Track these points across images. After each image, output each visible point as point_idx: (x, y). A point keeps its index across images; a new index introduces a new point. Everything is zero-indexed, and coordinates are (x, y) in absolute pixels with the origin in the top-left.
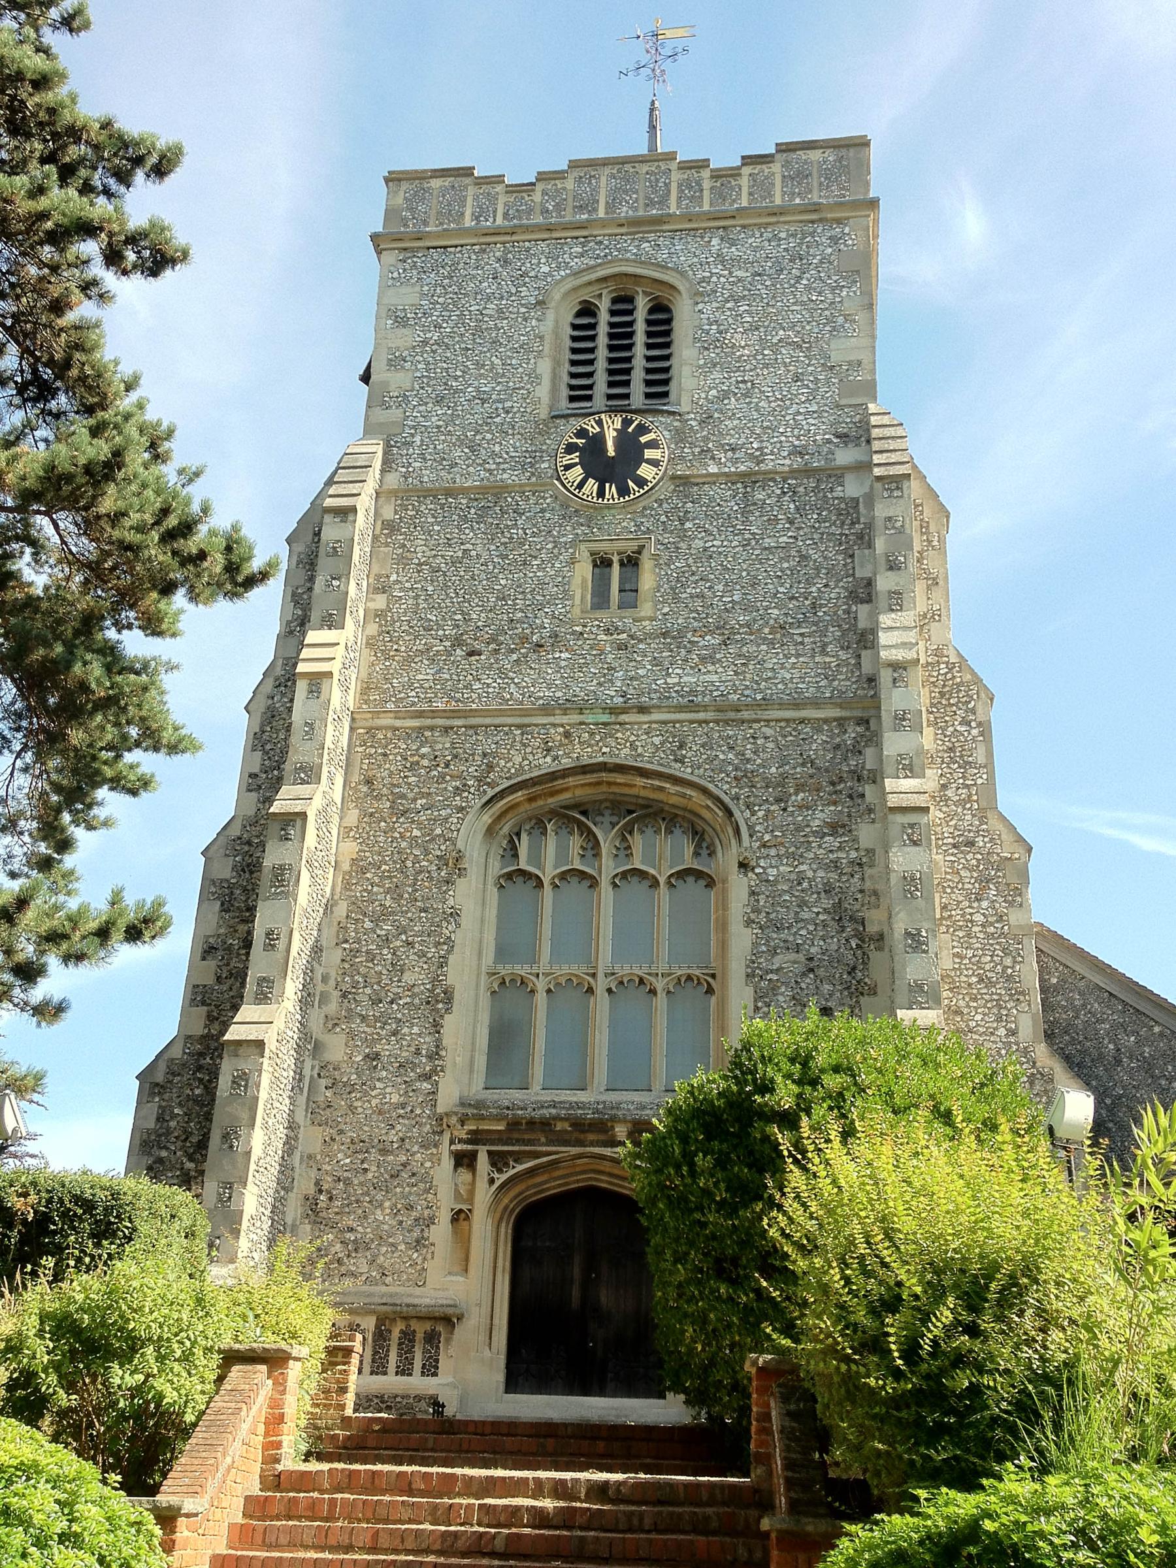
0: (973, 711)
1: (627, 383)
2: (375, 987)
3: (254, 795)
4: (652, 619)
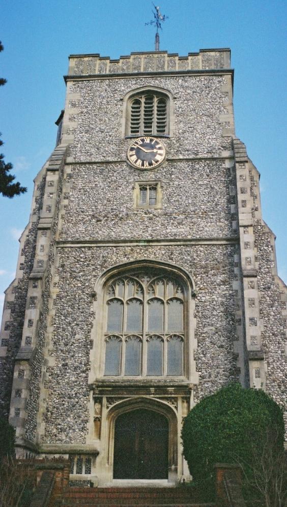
0: (269, 242)
1: (151, 127)
2: (66, 340)
3: (22, 271)
4: (161, 209)
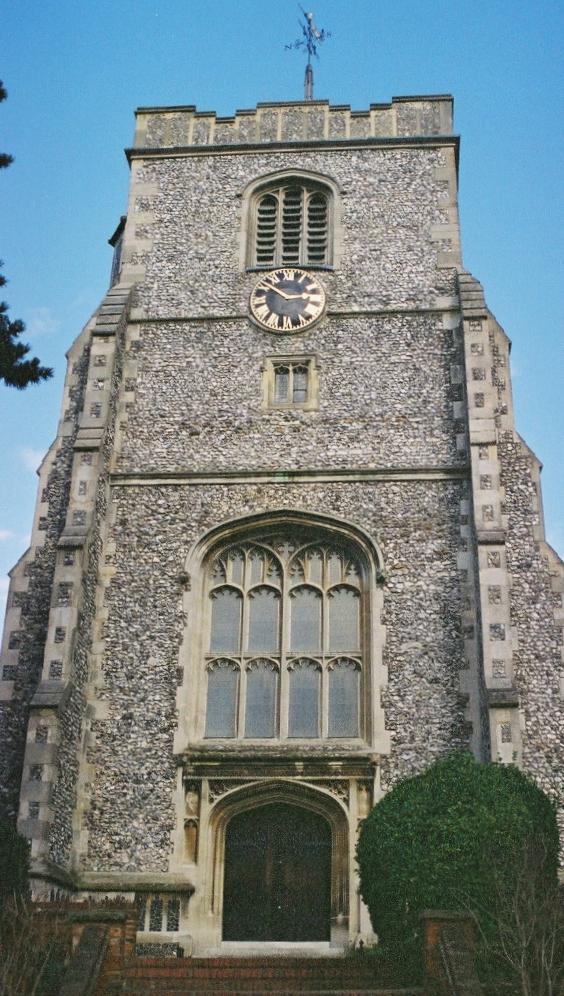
0: (529, 475)
1: (296, 249)
2: (129, 668)
3: (44, 532)
4: (316, 411)
